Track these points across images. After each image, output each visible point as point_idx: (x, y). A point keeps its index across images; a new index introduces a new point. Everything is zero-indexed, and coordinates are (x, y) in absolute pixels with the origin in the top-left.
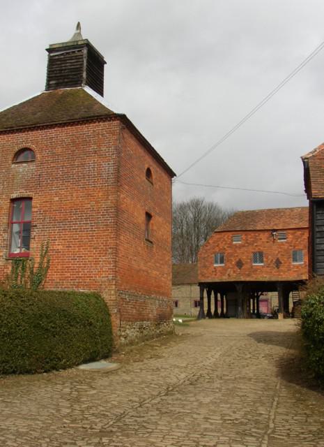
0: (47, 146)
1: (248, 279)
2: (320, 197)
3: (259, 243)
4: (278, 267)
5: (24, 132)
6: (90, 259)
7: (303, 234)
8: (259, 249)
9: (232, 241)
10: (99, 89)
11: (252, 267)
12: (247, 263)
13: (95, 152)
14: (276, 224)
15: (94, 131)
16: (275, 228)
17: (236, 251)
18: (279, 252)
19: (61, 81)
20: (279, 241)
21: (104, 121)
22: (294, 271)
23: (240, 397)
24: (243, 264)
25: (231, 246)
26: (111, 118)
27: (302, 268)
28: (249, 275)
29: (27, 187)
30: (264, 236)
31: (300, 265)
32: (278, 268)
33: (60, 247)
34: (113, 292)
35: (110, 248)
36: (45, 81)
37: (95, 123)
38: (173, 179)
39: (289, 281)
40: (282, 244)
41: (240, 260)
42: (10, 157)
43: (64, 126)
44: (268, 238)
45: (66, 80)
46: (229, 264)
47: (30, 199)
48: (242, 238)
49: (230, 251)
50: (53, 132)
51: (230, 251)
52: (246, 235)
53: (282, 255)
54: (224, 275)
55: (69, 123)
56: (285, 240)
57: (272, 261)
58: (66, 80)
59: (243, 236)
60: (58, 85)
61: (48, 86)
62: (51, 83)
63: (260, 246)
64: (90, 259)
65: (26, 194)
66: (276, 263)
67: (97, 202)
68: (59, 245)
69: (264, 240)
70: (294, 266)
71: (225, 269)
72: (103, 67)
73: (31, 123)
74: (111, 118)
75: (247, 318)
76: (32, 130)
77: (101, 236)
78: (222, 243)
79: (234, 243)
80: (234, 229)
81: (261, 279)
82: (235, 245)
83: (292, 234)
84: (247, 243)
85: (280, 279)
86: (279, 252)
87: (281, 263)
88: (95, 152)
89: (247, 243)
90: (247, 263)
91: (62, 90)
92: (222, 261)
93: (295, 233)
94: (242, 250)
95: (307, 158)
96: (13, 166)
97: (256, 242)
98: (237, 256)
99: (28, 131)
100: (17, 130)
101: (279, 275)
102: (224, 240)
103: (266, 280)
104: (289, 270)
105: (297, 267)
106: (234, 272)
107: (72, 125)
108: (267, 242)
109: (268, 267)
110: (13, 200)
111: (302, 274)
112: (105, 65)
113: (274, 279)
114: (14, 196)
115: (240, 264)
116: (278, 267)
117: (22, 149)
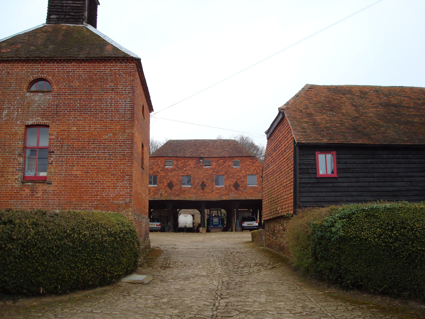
0: (63, 79)
1: (177, 198)
2: (303, 142)
3: (188, 168)
4: (203, 189)
5: (40, 63)
6: (109, 184)
7: (225, 162)
8: (188, 173)
9: (165, 165)
10: (95, 26)
11: (181, 188)
12: (177, 184)
13: (113, 90)
14: (202, 153)
15: (111, 70)
16: (202, 156)
17: (168, 174)
18: (204, 176)
19: (62, 16)
20: (204, 167)
21: (121, 62)
22: (217, 193)
23: (252, 291)
24: (174, 186)
25: (164, 170)
26: (127, 60)
27: (223, 190)
28: (178, 195)
29: (43, 116)
30: (192, 163)
31: (222, 188)
32: (203, 190)
33: (77, 173)
34: (130, 213)
35: (127, 175)
36: (46, 15)
37: (112, 62)
38: (151, 114)
39: (212, 201)
40: (207, 169)
41: (171, 182)
42: (25, 86)
43: (81, 62)
44: (195, 164)
45: (67, 17)
46: (161, 185)
47: (48, 126)
48: (173, 163)
49: (163, 174)
50: (70, 67)
51: (163, 174)
52: (177, 161)
53: (207, 179)
54: (157, 194)
55: (87, 60)
56: (210, 167)
57: (198, 183)
58: (67, 17)
59: (175, 162)
60: (59, 20)
61: (49, 19)
62: (52, 17)
63: (189, 170)
64: (109, 184)
65: (41, 121)
66: (201, 185)
67: (115, 134)
68: (77, 170)
69: (192, 166)
70: (217, 188)
71: (157, 189)
72: (97, 7)
73: (48, 56)
74: (127, 60)
75: (172, 232)
76: (48, 62)
77: (118, 164)
78: (156, 166)
79: (166, 167)
80: (166, 155)
81: (188, 199)
82: (167, 169)
83: (216, 162)
84: (178, 168)
85: (204, 199)
86: (204, 176)
87: (206, 186)
88: (113, 90)
89: (178, 168)
90: (177, 184)
91: (65, 25)
92: (155, 183)
93: (219, 161)
94: (173, 173)
95: (284, 110)
96: (28, 94)
97: (186, 168)
98: (169, 179)
99: (44, 62)
100: (33, 60)
101: (204, 195)
102: (158, 164)
103: (193, 199)
104: (212, 192)
105: (219, 189)
106: (166, 192)
107: (89, 62)
108: (195, 168)
109: (194, 188)
110: (28, 126)
111: (223, 195)
112: (98, 6)
113: (198, 199)
114: (30, 123)
115: (170, 185)
116: (203, 189)
117: (36, 80)
